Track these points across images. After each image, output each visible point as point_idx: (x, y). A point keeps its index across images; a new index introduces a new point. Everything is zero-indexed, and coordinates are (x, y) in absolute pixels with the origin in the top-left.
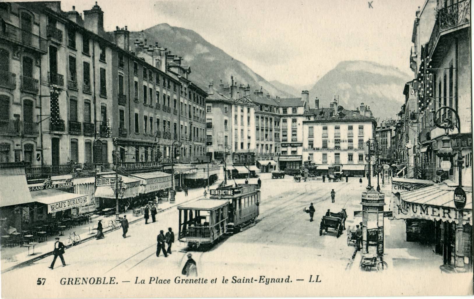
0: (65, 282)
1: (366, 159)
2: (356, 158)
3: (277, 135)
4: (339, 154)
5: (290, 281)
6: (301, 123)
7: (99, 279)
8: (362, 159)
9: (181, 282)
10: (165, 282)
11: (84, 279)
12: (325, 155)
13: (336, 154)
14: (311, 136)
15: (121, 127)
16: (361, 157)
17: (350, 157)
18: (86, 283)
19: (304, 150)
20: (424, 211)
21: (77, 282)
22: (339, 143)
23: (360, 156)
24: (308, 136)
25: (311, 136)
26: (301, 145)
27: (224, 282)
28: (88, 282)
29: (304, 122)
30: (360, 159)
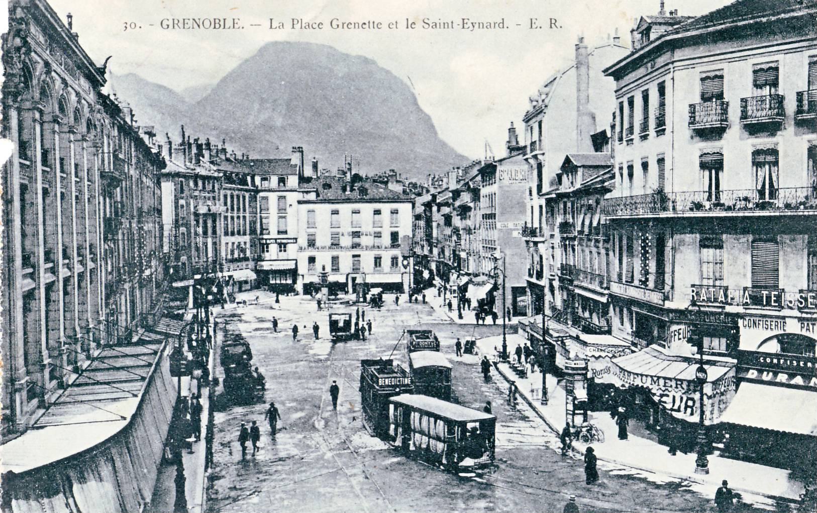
0: (168, 26)
1: (403, 265)
2: (386, 262)
4: (359, 256)
5: (505, 26)
8: (397, 264)
9: (341, 26)
11: (194, 19)
13: (354, 256)
14: (311, 225)
16: (394, 260)
17: (378, 261)
18: (199, 26)
20: (655, 383)
22: (359, 237)
24: (307, 226)
25: (311, 225)
29: (299, 202)
30: (393, 265)
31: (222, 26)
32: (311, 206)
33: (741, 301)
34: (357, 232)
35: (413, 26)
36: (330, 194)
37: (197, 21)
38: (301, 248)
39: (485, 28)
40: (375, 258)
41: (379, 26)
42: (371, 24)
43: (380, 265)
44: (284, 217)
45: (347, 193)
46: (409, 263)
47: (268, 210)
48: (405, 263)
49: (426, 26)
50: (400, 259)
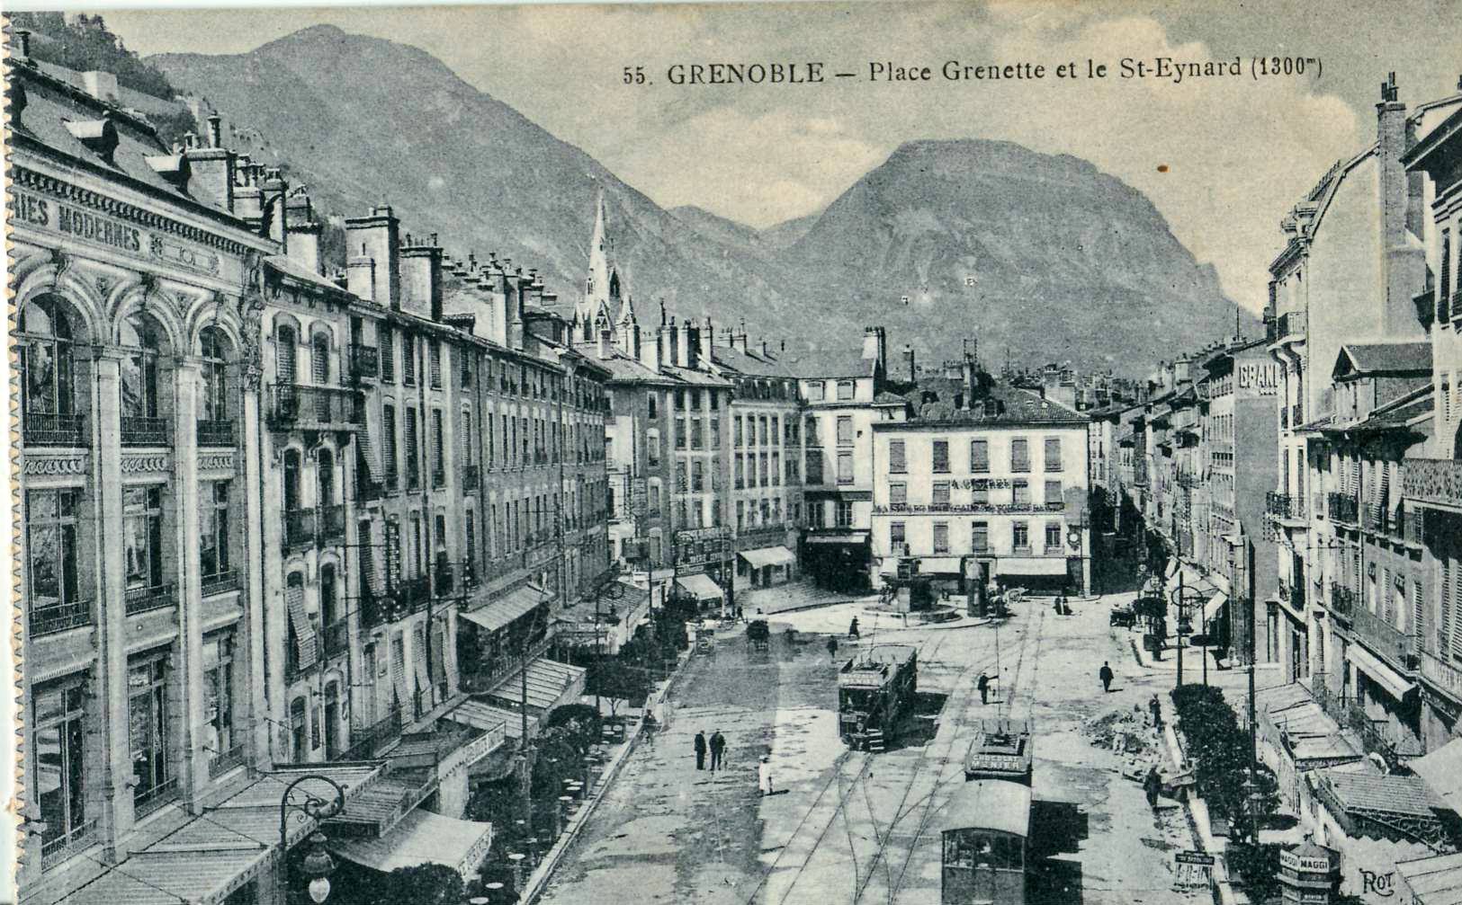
1: (1069, 541)
2: (1037, 536)
3: (792, 468)
4: (984, 524)
6: (867, 430)
7: (777, 69)
9: (962, 75)
10: (757, 74)
11: (731, 67)
12: (940, 528)
13: (975, 524)
15: (288, 506)
16: (1052, 532)
17: (1020, 535)
18: (741, 78)
19: (878, 510)
21: (814, 75)
23: (1048, 530)
26: (866, 495)
27: (1094, 73)
28: (746, 78)
29: (877, 428)
31: (787, 77)
32: (896, 435)
33: (707, 415)
34: (981, 481)
35: (1102, 73)
36: (932, 412)
37: (738, 68)
38: (878, 509)
39: (1023, 64)
40: (1015, 529)
41: (1040, 73)
42: (1023, 71)
43: (1025, 541)
44: (848, 454)
45: (963, 409)
46: (1080, 540)
47: (1047, 483)
48: (1074, 538)
49: (1128, 73)
50: (1064, 530)
